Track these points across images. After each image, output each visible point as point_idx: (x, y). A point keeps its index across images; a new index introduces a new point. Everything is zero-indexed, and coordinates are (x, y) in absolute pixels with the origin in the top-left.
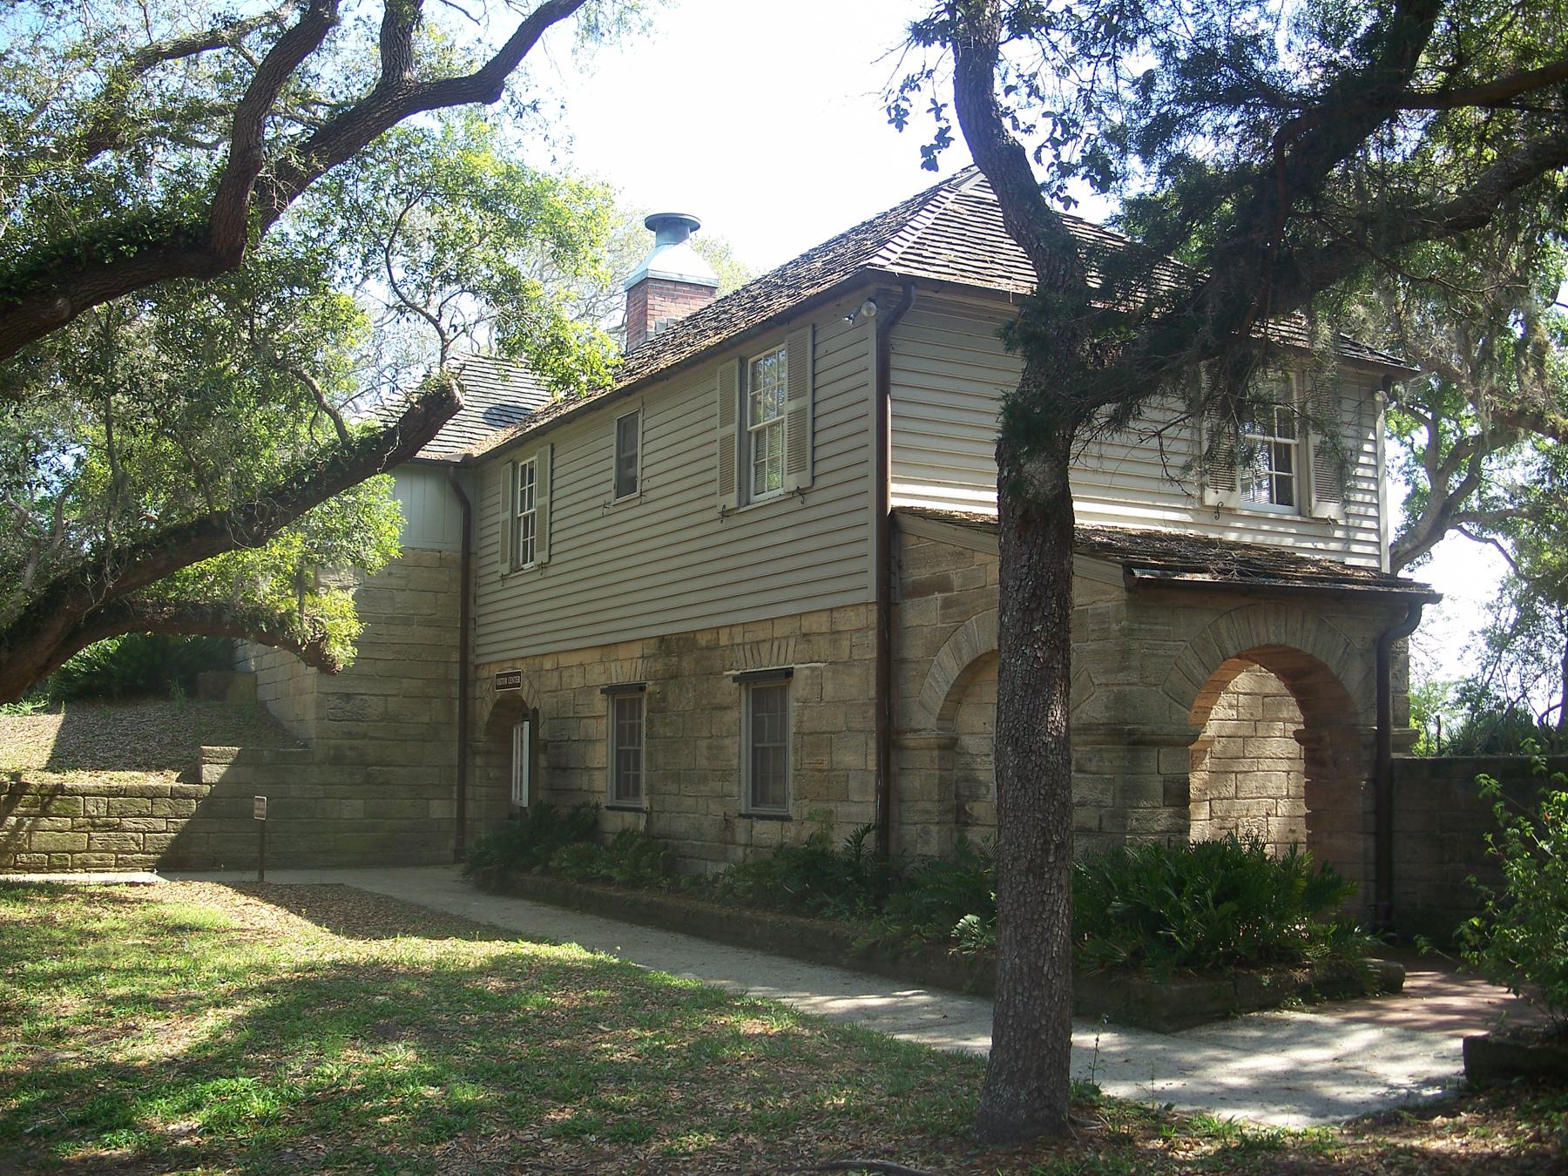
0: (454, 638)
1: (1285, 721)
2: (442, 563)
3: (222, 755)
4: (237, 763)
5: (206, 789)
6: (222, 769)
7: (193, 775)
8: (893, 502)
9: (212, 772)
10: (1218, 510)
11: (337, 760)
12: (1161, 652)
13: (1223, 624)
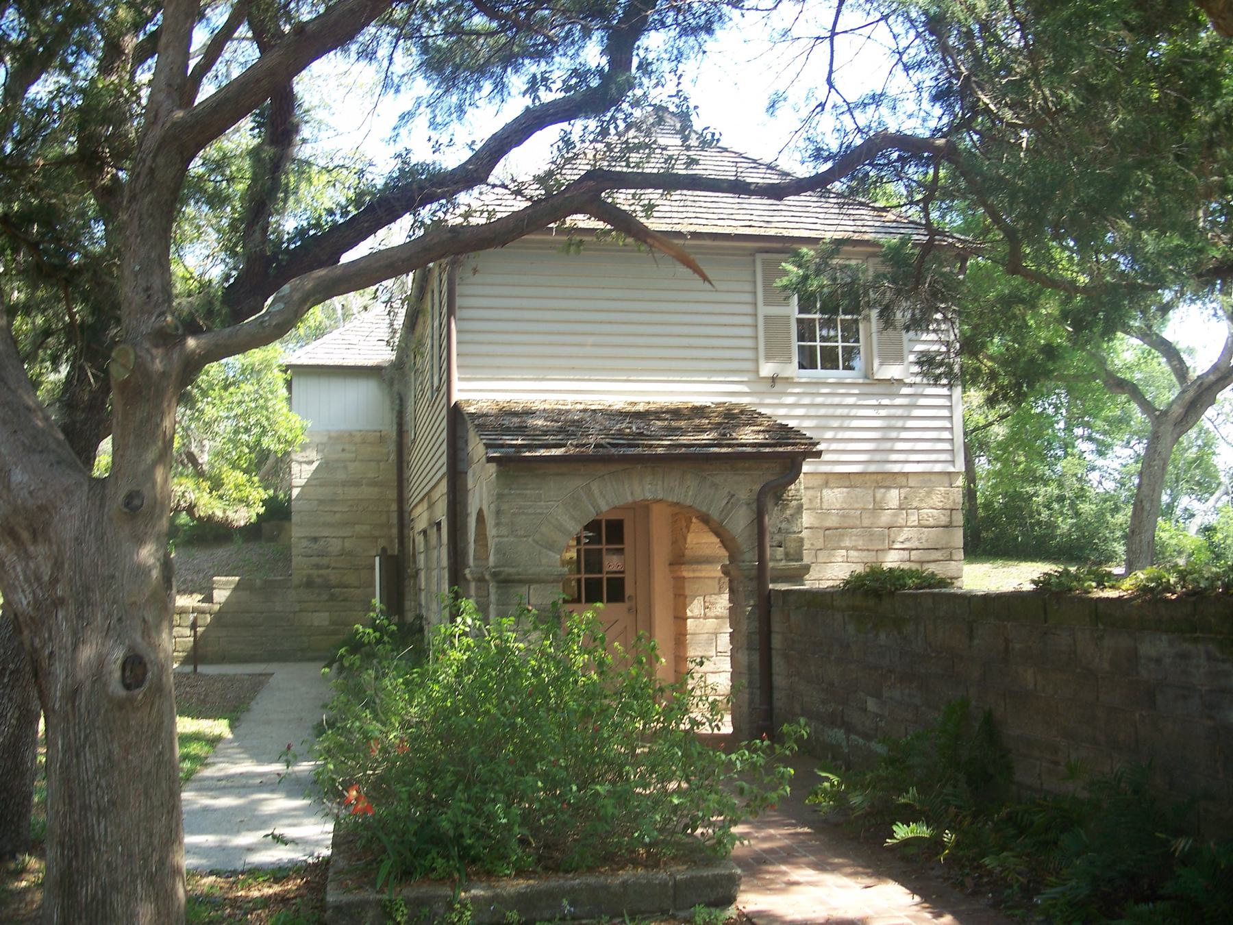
0: (392, 494)
1: (847, 549)
2: (382, 439)
3: (227, 583)
4: (238, 588)
5: (217, 607)
6: (227, 593)
7: (209, 599)
8: (456, 397)
9: (221, 595)
10: (774, 380)
11: (309, 584)
12: (530, 511)
13: (595, 487)
